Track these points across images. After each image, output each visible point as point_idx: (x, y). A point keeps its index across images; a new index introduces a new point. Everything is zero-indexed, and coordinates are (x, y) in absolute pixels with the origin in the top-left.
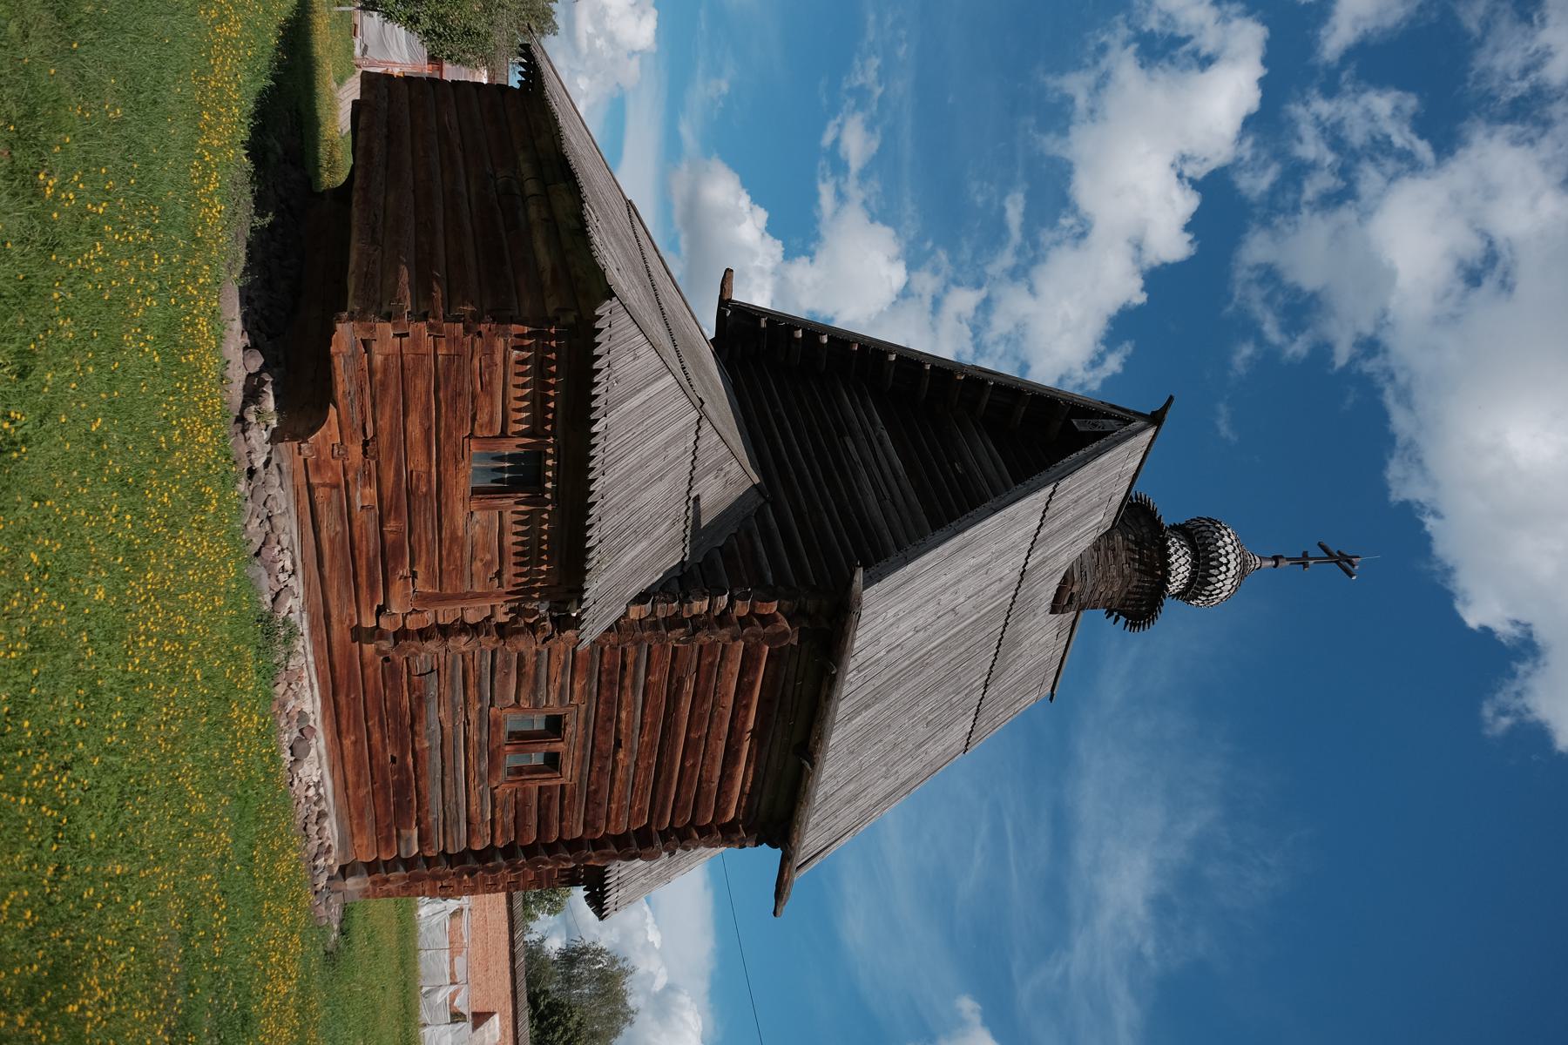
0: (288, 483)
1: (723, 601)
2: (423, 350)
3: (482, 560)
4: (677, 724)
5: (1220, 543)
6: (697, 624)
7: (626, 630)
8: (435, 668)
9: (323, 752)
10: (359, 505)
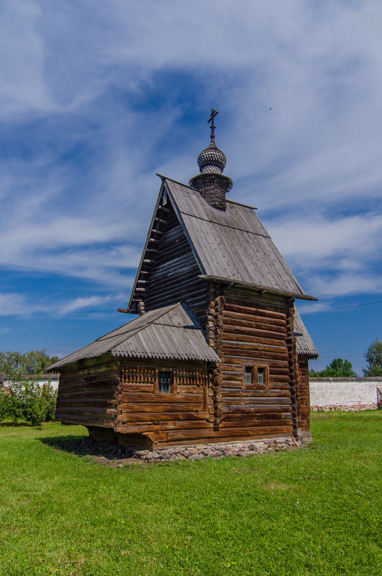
0: (166, 447)
1: (210, 317)
2: (126, 407)
3: (193, 390)
4: (254, 332)
5: (205, 156)
6: (217, 326)
7: (217, 347)
8: (227, 405)
9: (254, 441)
10: (174, 427)
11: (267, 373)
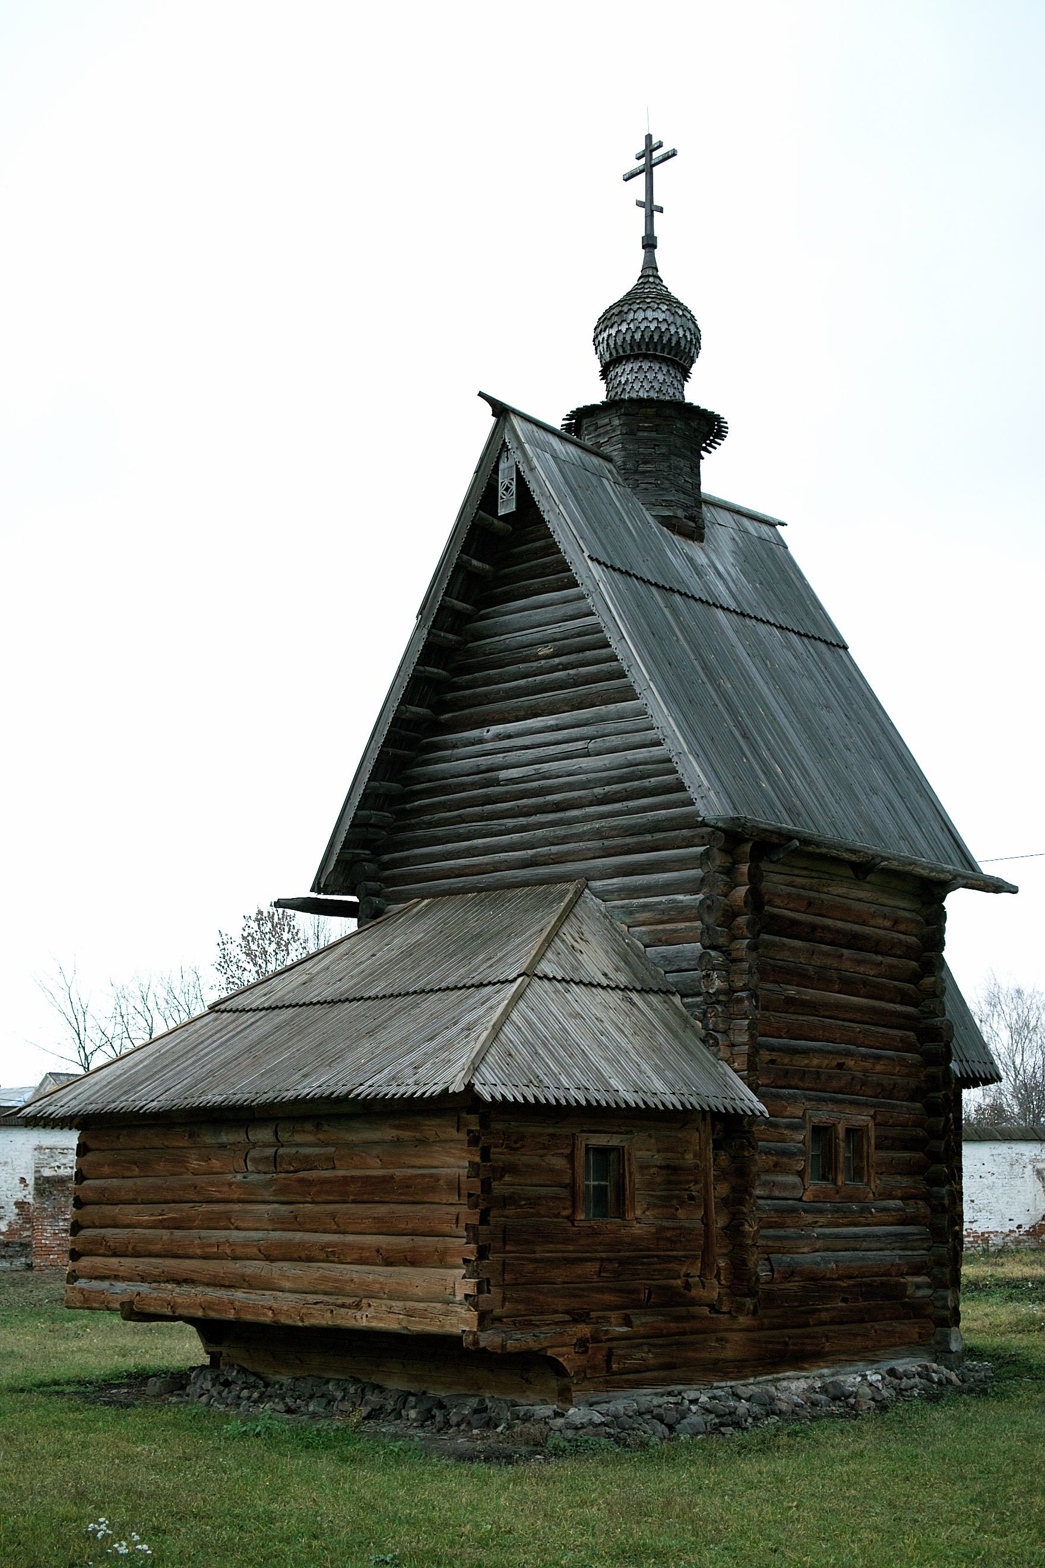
11: (869, 1143)
